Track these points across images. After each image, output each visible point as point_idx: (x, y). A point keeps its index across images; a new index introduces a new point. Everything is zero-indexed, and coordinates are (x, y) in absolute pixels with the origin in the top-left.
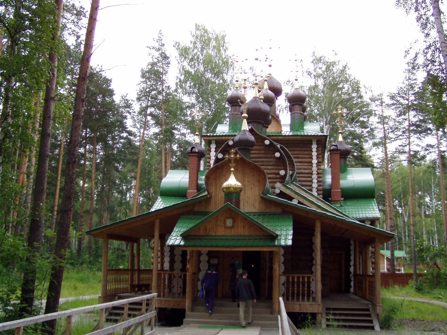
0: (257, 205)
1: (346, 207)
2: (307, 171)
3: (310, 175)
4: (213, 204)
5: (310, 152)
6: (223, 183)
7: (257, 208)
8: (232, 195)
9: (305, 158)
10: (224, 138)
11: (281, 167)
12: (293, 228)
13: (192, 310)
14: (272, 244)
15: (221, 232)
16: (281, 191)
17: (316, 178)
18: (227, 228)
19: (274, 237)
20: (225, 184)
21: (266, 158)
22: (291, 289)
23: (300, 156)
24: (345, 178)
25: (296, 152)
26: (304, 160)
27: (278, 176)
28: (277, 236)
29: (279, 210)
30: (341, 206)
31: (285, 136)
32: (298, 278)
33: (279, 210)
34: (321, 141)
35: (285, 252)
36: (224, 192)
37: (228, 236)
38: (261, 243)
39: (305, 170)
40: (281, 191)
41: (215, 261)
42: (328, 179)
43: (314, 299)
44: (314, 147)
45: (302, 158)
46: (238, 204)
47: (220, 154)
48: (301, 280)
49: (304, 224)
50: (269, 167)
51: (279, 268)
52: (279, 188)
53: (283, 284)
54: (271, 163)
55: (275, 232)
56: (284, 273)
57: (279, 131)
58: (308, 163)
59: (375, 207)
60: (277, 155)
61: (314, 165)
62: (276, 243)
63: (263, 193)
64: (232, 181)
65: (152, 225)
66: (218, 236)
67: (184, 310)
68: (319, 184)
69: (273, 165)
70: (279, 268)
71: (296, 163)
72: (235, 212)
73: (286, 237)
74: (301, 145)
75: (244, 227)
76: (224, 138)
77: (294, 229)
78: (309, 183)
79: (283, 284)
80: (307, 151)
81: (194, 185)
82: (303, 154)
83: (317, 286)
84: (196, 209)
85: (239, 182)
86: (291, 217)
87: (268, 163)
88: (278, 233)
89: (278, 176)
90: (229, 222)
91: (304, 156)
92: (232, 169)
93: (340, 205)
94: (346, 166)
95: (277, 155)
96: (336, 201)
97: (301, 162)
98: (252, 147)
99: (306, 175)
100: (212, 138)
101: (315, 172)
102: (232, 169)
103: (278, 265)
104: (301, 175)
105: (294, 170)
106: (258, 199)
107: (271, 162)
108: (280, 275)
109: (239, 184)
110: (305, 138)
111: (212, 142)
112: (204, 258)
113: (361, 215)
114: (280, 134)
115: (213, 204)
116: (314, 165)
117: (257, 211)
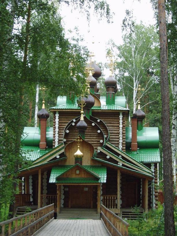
0: (89, 162)
1: (140, 155)
2: (116, 132)
3: (118, 134)
4: (68, 162)
5: (118, 120)
6: (74, 153)
7: (89, 164)
8: (79, 159)
9: (115, 123)
10: (64, 110)
11: (101, 138)
12: (107, 174)
13: (60, 213)
14: (97, 182)
15: (74, 176)
16: (100, 151)
17: (122, 136)
18: (77, 174)
19: (98, 179)
20: (75, 154)
21: (92, 132)
22: (105, 202)
23: (112, 122)
24: (141, 135)
25: (109, 120)
26: (114, 125)
27: (99, 143)
28: (100, 178)
29: (100, 165)
30: (137, 153)
31: (103, 110)
32: (109, 197)
33: (100, 165)
34: (126, 114)
35: (102, 188)
36: (75, 157)
37: (77, 178)
38: (94, 182)
39: (115, 131)
40: (100, 151)
41: (67, 189)
42: (130, 135)
43: (116, 208)
44: (121, 117)
45: (113, 123)
46: (81, 163)
47: (67, 130)
48: (110, 198)
49: (112, 172)
50: (94, 138)
51: (100, 192)
52: (100, 150)
53: (102, 201)
54: (96, 135)
55: (98, 176)
56: (102, 195)
57: (99, 105)
58: (117, 127)
59: (157, 153)
60: (99, 131)
61: (121, 128)
62: (99, 182)
63: (92, 157)
64: (79, 153)
65: (38, 171)
66: (72, 178)
67: (56, 213)
68: (123, 140)
69: (96, 137)
70: (100, 192)
71: (109, 131)
72: (80, 167)
73: (103, 178)
74: (113, 115)
75: (84, 174)
76: (64, 110)
77: (107, 175)
78: (117, 140)
79: (102, 201)
80: (117, 119)
81: (44, 139)
82: (114, 121)
83: (119, 202)
84: (59, 164)
85: (82, 152)
86: (106, 168)
87: (94, 135)
88: (100, 177)
89: (99, 143)
90: (78, 172)
91: (114, 122)
92: (79, 146)
93: (136, 153)
94: (142, 126)
95: (99, 131)
96: (134, 150)
97: (113, 126)
98: (86, 129)
99: (115, 134)
100: (56, 110)
101: (121, 133)
102: (79, 146)
103: (99, 191)
104: (112, 134)
105: (108, 134)
106: (90, 159)
107: (95, 134)
108: (100, 196)
109: (82, 154)
110: (115, 111)
111: (56, 112)
112: (62, 188)
113: (148, 160)
114: (100, 109)
115: (68, 162)
116: (121, 128)
117: (89, 165)
